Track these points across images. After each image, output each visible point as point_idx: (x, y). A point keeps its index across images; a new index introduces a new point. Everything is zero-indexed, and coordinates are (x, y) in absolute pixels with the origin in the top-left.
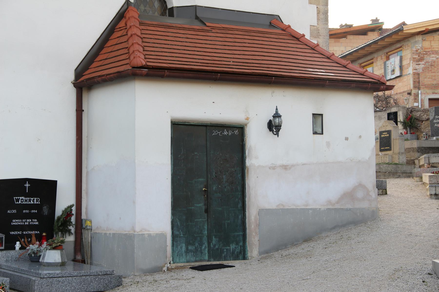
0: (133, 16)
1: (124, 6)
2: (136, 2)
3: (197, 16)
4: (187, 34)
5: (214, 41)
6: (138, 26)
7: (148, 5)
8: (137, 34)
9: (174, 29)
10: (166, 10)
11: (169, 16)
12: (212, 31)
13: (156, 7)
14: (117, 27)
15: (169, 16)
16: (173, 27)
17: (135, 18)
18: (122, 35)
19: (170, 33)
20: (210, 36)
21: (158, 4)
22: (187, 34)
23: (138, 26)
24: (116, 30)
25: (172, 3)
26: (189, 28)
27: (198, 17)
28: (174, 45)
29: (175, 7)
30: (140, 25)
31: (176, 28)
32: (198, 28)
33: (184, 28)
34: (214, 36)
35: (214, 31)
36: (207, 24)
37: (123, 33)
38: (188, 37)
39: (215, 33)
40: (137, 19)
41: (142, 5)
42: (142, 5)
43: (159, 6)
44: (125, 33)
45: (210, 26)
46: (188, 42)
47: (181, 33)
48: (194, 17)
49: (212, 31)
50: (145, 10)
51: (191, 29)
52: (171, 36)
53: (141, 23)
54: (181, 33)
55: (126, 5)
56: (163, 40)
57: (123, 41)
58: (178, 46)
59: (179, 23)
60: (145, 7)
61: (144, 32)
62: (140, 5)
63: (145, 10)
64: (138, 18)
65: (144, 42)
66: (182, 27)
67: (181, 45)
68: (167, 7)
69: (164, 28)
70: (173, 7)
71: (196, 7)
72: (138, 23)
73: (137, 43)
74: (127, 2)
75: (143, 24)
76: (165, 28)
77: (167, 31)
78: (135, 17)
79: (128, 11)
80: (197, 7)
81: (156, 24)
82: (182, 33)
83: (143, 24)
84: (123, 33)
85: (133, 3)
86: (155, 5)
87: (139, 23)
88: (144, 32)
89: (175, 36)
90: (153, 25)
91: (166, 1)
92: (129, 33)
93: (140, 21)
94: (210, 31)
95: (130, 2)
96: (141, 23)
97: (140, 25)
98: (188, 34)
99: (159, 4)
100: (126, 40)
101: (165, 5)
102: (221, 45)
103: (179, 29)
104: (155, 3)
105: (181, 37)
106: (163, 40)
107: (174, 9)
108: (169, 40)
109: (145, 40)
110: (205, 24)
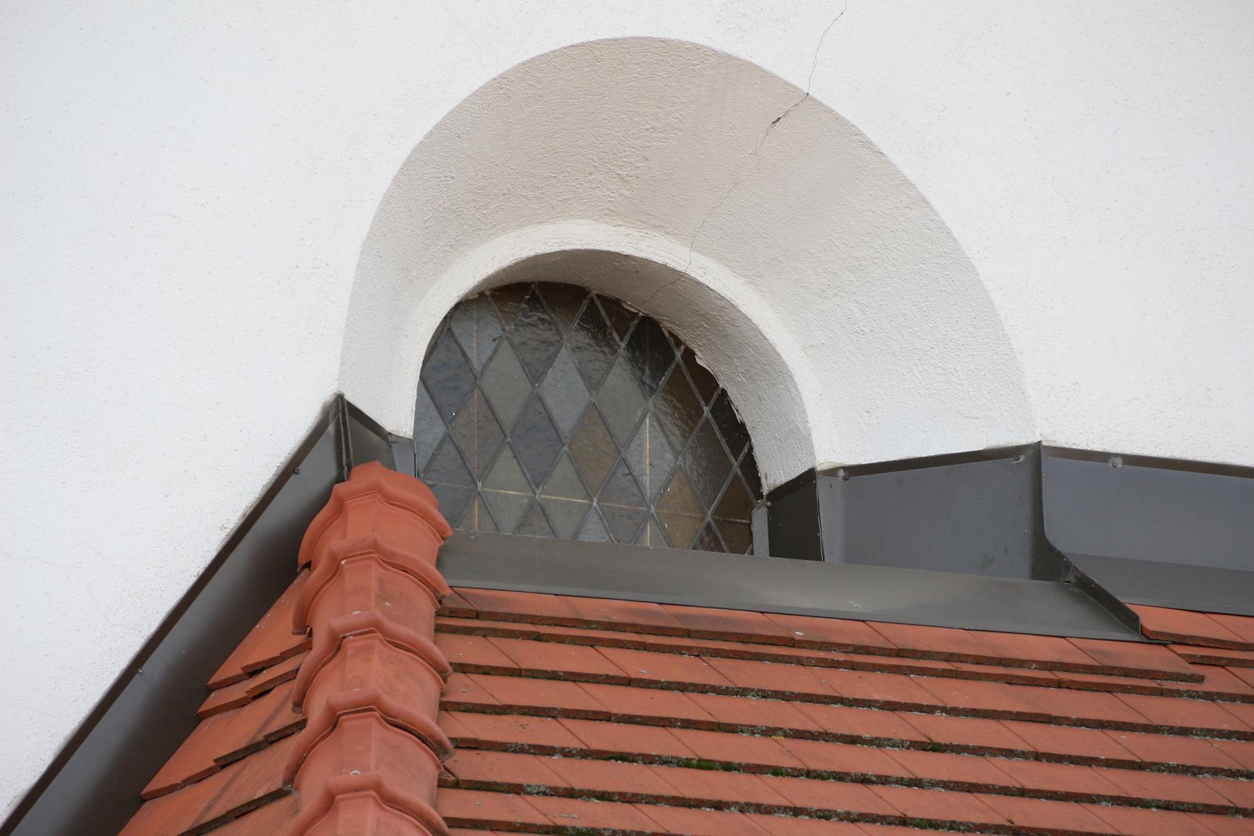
0: (375, 547)
1: (303, 467)
2: (447, 438)
3: (1051, 549)
4: (930, 710)
5: (1215, 772)
6: (424, 638)
7: (564, 469)
8: (394, 703)
9: (800, 662)
10: (745, 510)
11: (774, 552)
12: (1200, 679)
13: (646, 481)
14: (233, 666)
15: (774, 552)
16: (792, 643)
17: (390, 561)
18: (261, 738)
19: (752, 700)
20: (1172, 731)
21: (669, 456)
22: (930, 710)
23: (424, 638)
24: (214, 700)
25: (805, 441)
26: (950, 657)
27: (1060, 556)
28: (785, 810)
29: (832, 472)
30: (439, 629)
31: (822, 654)
32: (1045, 650)
33: (900, 653)
34: (1226, 727)
35: (1216, 680)
36: (1154, 619)
37: (272, 718)
38: (937, 739)
39: (1233, 698)
40: (417, 576)
41: (506, 467)
42: (506, 467)
43: (672, 474)
44: (287, 717)
45: (1182, 641)
46: (934, 784)
47: (868, 704)
48: (1023, 563)
49: (1200, 679)
50: (536, 511)
51: (979, 660)
52: (761, 722)
53: (453, 614)
54: (868, 704)
55: (323, 463)
56: (665, 762)
57: (260, 793)
58: (827, 818)
59: (856, 605)
60: (537, 479)
61: (466, 689)
62: (488, 468)
63: (536, 511)
64: (432, 568)
65: (457, 785)
66: (879, 642)
67: (856, 809)
68: (755, 481)
69: (689, 650)
70: (809, 477)
71: (1036, 453)
72: (426, 607)
73: (378, 788)
74: (331, 429)
75: (478, 615)
76: (699, 653)
77: (724, 684)
78: (392, 554)
79: (340, 509)
80: (1046, 461)
81: (615, 618)
82: (876, 696)
83: (478, 615)
84: (272, 718)
85: (409, 442)
86: (632, 460)
87: (439, 614)
88: (466, 689)
89: (800, 727)
90: (587, 624)
91: (742, 427)
92: (316, 712)
93: (448, 592)
94: (1182, 686)
95: (375, 438)
96: (453, 614)
97: (439, 629)
98: (944, 710)
99: (676, 454)
100: (277, 784)
101: (735, 464)
102: (1228, 735)
103: (853, 666)
104: (641, 445)
105: (867, 735)
106: (665, 762)
107: (822, 486)
108: (735, 760)
109: (467, 765)
110: (1129, 620)
